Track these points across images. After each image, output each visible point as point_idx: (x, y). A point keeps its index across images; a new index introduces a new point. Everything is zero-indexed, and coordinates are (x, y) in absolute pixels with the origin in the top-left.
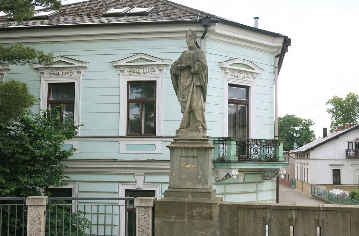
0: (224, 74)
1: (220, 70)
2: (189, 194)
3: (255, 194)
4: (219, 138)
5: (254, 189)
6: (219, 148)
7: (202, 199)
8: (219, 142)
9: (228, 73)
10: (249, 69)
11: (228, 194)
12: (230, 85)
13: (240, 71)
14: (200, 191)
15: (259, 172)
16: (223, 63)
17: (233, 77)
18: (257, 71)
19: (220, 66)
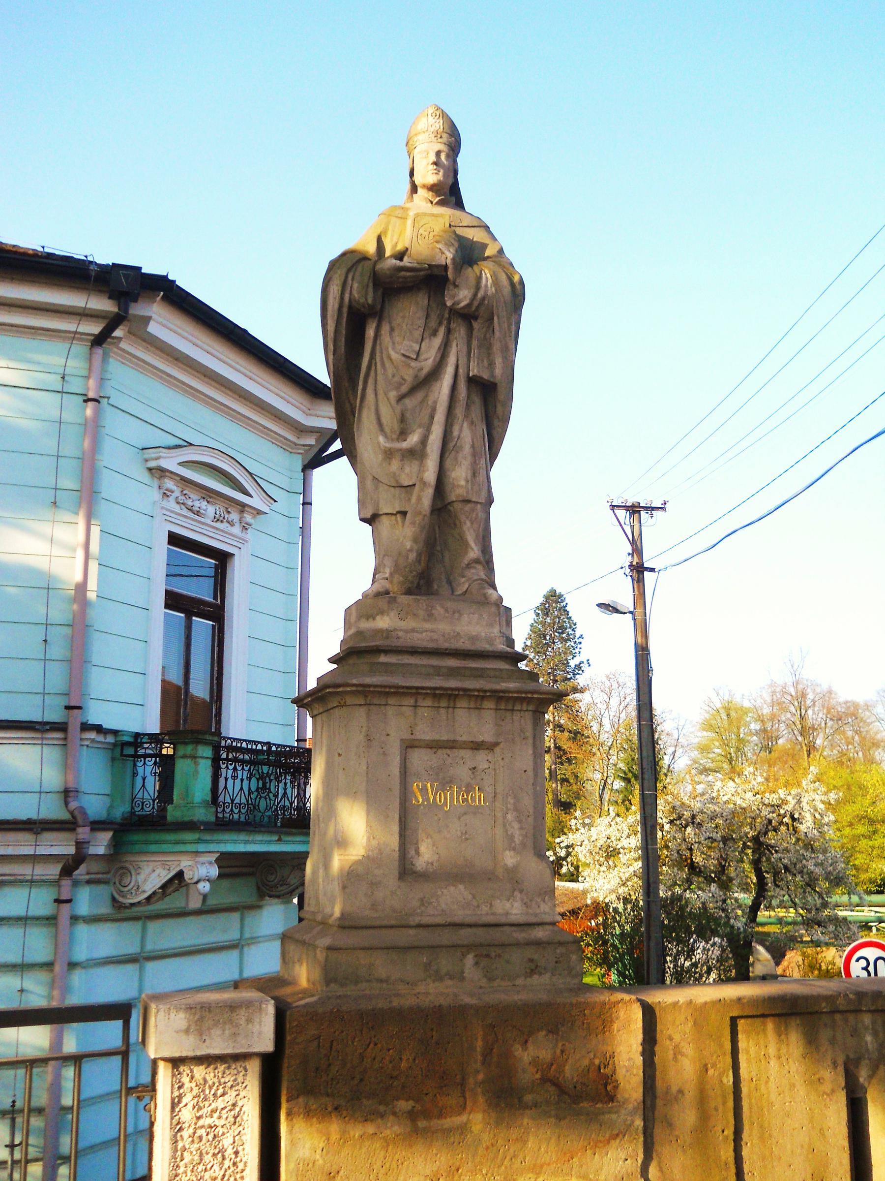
0: (156, 495)
1: (146, 477)
2: (470, 959)
3: (235, 953)
4: (137, 735)
5: (233, 935)
6: (135, 774)
7: (536, 980)
8: (136, 751)
9: (173, 492)
10: (224, 488)
11: (149, 959)
12: (175, 539)
13: (209, 494)
14: (520, 935)
15: (251, 870)
16: (164, 453)
17: (185, 512)
18: (256, 501)
19: (147, 461)
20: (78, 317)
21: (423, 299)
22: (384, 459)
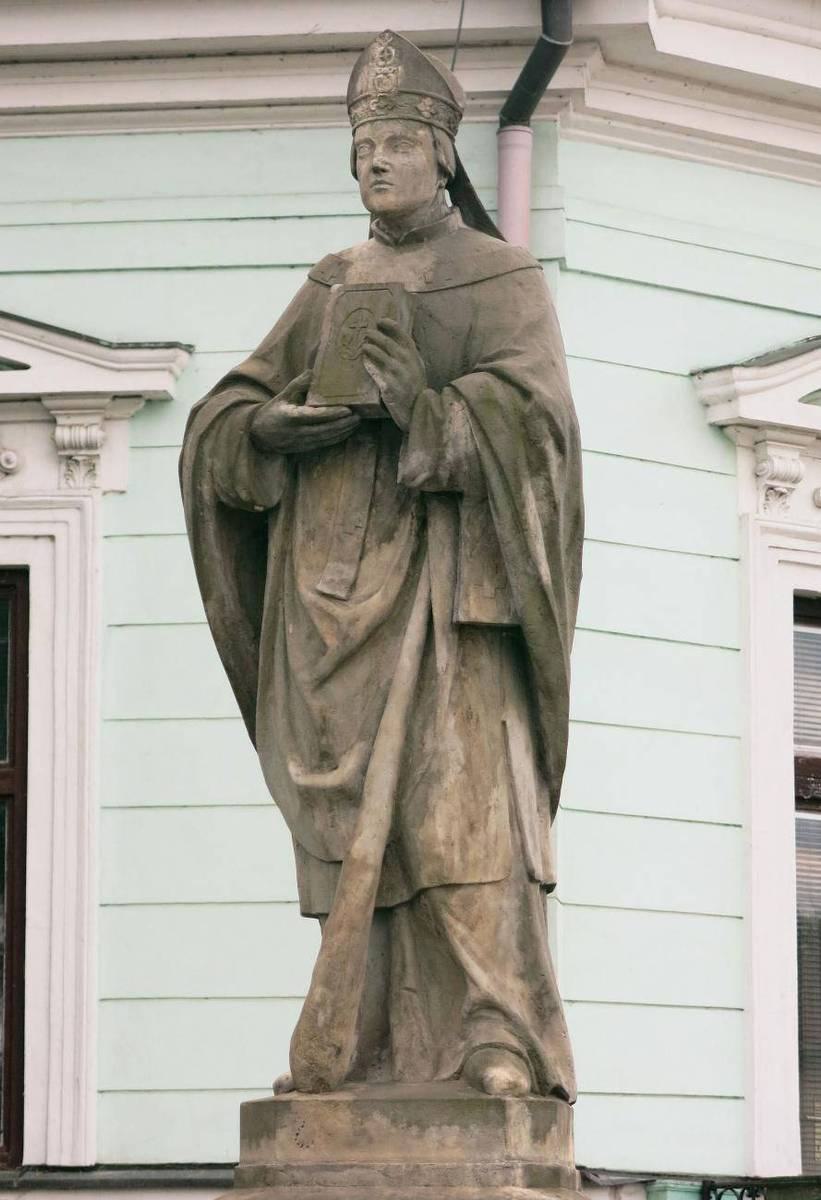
0: (748, 496)
1: (709, 452)
16: (744, 379)
20: (464, 38)
21: (363, 466)
22: (303, 807)
